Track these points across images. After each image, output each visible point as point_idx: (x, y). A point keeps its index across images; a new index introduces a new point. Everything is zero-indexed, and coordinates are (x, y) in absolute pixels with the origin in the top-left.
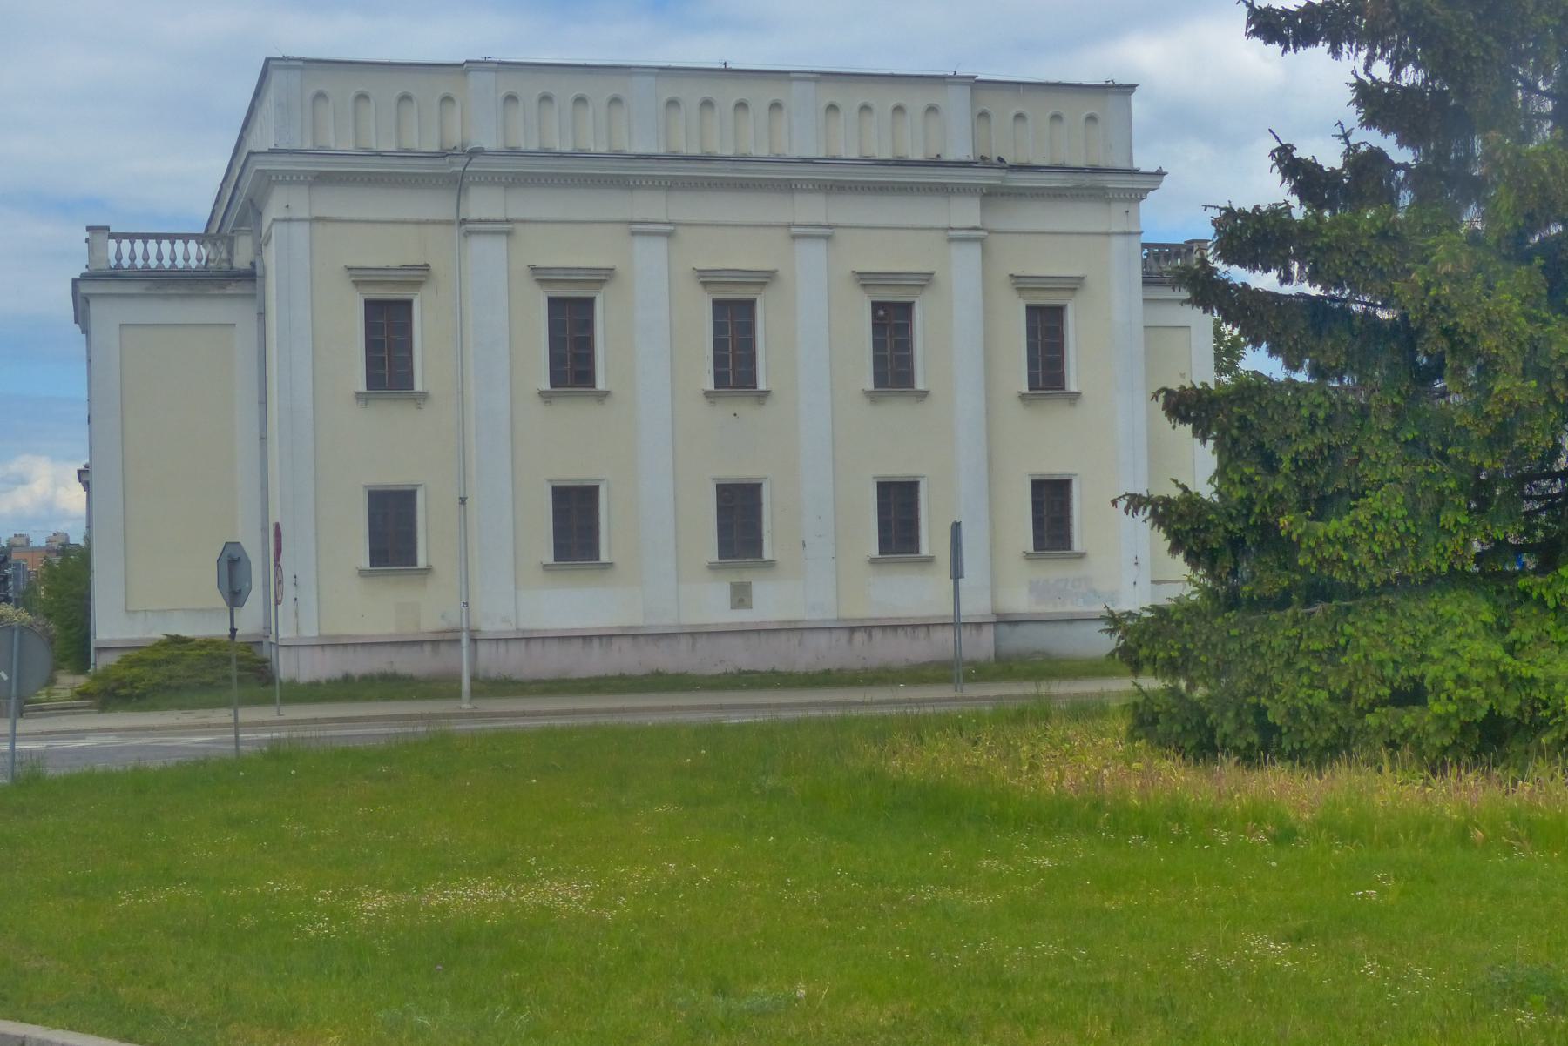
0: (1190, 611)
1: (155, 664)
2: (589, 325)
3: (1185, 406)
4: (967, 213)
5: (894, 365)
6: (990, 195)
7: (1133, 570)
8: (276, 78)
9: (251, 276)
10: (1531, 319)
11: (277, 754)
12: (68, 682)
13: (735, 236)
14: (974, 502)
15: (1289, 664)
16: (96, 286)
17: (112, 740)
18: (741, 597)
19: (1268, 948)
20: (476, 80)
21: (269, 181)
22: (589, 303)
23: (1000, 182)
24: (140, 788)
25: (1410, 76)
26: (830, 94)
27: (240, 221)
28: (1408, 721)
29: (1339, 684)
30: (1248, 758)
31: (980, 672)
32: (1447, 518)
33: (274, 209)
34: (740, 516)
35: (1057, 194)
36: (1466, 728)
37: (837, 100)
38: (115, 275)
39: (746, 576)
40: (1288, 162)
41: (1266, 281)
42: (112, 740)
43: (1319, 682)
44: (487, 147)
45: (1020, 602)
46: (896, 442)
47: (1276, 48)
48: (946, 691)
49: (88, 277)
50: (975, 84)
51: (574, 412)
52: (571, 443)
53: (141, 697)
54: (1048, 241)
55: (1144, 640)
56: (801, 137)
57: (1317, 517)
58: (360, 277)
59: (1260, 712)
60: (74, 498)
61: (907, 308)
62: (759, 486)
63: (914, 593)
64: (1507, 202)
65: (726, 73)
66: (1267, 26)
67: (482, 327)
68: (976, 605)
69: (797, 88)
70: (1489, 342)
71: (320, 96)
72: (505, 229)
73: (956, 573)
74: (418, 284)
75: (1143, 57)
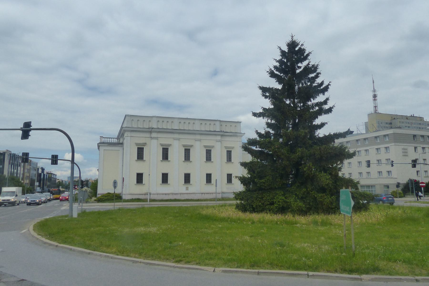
0: (244, 192)
1: (106, 196)
2: (168, 151)
3: (244, 164)
4: (219, 138)
5: (187, 157)
6: (222, 136)
7: (239, 187)
8: (127, 117)
9: (122, 144)
10: (288, 154)
11: (119, 209)
12: (94, 198)
13: (188, 140)
14: (219, 177)
15: (256, 199)
16: (99, 145)
17: (98, 207)
18: (187, 189)
19: (247, 238)
21: (125, 131)
22: (168, 149)
23: (223, 134)
24: (99, 214)
25: (273, 122)
26: (201, 122)
27: (121, 136)
28: (272, 207)
29: (263, 202)
30: (251, 212)
31: (219, 200)
32: (277, 180)
33: (126, 135)
34: (187, 178)
35: (231, 136)
36: (279, 208)
38: (103, 143)
39: (188, 186)
40: (257, 133)
41: (254, 148)
42: (98, 207)
43: (260, 202)
44: (154, 127)
45: (225, 190)
46: (209, 168)
47: (256, 117)
48: (215, 202)
49: (100, 143)
50: (220, 121)
51: (165, 163)
52: (165, 167)
53: (104, 201)
54: (230, 142)
55: (238, 196)
56: (197, 127)
57: (260, 179)
58: (137, 144)
59: (252, 205)
60: (97, 173)
61: (211, 150)
63: (211, 188)
64: (285, 138)
65: (187, 119)
66: (255, 114)
67: (153, 152)
68: (219, 190)
69: (196, 121)
70: (282, 157)
72: (157, 138)
73: (216, 186)
74: (145, 145)
75: (241, 118)
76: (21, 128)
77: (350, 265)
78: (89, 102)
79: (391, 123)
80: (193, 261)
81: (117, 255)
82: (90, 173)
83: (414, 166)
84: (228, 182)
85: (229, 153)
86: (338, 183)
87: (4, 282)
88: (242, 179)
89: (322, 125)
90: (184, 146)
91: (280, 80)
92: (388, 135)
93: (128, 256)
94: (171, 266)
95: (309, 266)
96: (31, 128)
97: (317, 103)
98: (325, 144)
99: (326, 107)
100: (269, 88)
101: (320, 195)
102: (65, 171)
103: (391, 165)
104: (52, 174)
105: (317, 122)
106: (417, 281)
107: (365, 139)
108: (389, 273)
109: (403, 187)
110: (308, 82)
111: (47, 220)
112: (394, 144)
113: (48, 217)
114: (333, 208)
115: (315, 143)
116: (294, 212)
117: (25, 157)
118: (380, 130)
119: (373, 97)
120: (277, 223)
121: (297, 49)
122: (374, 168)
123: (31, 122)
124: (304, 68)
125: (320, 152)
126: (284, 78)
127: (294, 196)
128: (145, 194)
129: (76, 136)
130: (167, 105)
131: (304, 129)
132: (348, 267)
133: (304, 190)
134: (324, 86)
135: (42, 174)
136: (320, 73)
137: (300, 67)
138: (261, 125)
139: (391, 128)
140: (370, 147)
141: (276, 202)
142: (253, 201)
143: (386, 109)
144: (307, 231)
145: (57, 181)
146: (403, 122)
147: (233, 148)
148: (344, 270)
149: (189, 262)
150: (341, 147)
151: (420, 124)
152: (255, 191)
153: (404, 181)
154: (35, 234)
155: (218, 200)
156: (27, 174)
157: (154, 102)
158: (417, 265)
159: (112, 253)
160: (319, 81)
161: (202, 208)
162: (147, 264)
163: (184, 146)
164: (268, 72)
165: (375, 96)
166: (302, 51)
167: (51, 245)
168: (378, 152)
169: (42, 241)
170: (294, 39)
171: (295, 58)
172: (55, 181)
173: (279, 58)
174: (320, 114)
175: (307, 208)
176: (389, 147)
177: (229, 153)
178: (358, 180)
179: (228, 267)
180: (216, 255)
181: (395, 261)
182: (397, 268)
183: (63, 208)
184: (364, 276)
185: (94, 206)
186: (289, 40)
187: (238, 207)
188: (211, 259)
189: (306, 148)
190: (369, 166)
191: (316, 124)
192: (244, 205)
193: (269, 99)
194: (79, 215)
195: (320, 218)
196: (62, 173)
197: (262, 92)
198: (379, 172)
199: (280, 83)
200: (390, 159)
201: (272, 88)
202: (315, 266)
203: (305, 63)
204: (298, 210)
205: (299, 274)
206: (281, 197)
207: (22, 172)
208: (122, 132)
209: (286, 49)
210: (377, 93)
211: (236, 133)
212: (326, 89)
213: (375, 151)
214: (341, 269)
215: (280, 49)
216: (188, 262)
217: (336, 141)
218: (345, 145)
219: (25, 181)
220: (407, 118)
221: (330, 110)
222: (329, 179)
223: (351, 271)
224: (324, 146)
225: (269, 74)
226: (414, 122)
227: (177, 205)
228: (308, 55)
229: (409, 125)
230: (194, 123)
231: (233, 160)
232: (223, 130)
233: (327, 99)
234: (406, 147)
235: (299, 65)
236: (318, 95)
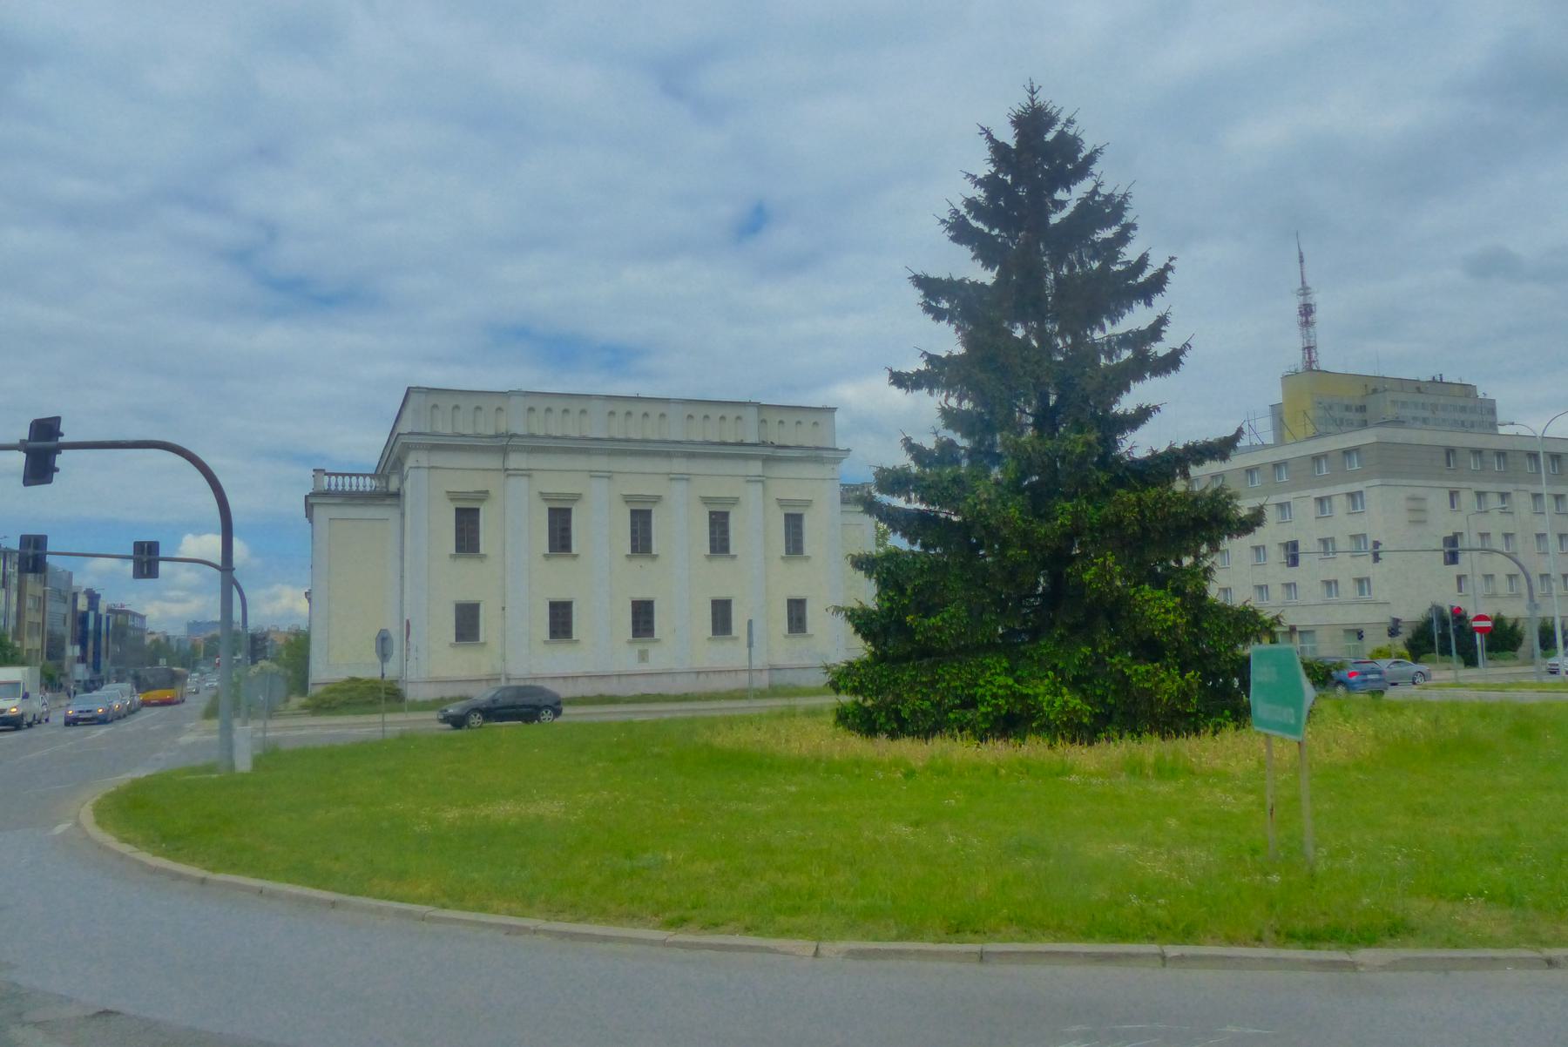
0: (865, 664)
2: (568, 521)
3: (864, 564)
4: (755, 468)
6: (767, 460)
9: (397, 495)
10: (1024, 521)
11: (402, 737)
12: (296, 701)
13: (642, 478)
14: (759, 610)
15: (912, 689)
18: (643, 656)
19: (903, 830)
21: (407, 448)
22: (568, 511)
23: (771, 454)
25: (967, 405)
27: (394, 467)
28: (969, 716)
30: (893, 735)
31: (761, 694)
32: (986, 617)
33: (410, 462)
34: (643, 617)
36: (996, 719)
38: (327, 494)
40: (910, 446)
41: (899, 502)
43: (925, 697)
45: (780, 660)
46: (721, 579)
47: (903, 391)
49: (313, 495)
50: (759, 406)
52: (560, 579)
54: (795, 483)
55: (843, 678)
56: (595, 427)
58: (453, 496)
59: (897, 712)
60: (303, 607)
63: (730, 654)
64: (1012, 465)
65: (638, 399)
66: (899, 380)
70: (1005, 532)
72: (527, 473)
73: (750, 645)
74: (482, 500)
76: (22, 441)
77: (1321, 925)
78: (276, 338)
79: (1362, 409)
80: (732, 920)
81: (444, 907)
82: (278, 605)
83: (1452, 558)
84: (791, 630)
85: (794, 524)
86: (1206, 625)
87: (36, 1024)
88: (859, 617)
89: (1143, 414)
90: (628, 499)
91: (987, 251)
92: (1357, 449)
93: (483, 909)
94: (653, 943)
95: (1159, 926)
96: (61, 440)
97: (1125, 335)
98: (1154, 485)
99: (1160, 349)
100: (950, 282)
101: (1142, 669)
102: (178, 601)
103: (1371, 557)
104: (127, 613)
105: (1126, 404)
106: (1550, 963)
107: (1277, 466)
108: (1449, 940)
109: (1410, 636)
110: (1092, 258)
111: (138, 786)
112: (1377, 482)
113: (140, 773)
114: (1190, 715)
115: (1120, 482)
116: (1050, 730)
117: (30, 552)
118: (1328, 434)
119: (1301, 314)
120: (996, 772)
121: (1049, 137)
122: (1310, 571)
123: (57, 420)
124: (1078, 208)
125: (1141, 512)
126: (1004, 244)
127: (1051, 674)
128: (565, 678)
129: (218, 468)
130: (563, 348)
131: (1080, 431)
132: (1300, 926)
133: (1086, 650)
134: (1148, 273)
135: (92, 614)
136: (1133, 226)
137: (1061, 205)
138: (924, 417)
139: (1364, 424)
140: (1294, 495)
141: (983, 696)
142: (899, 696)
143: (1342, 356)
144: (1109, 797)
145: (148, 640)
146: (1404, 404)
147: (808, 503)
148: (1291, 937)
149: (716, 925)
150: (1216, 493)
151: (1463, 409)
152: (907, 658)
153: (1413, 611)
154: (110, 840)
155: (756, 697)
156: (32, 617)
157: (519, 335)
158: (1538, 907)
159: (419, 900)
160: (1131, 253)
161: (711, 724)
162: (563, 935)
163: (628, 499)
164: (943, 221)
165: (1307, 311)
166: (1068, 144)
167: (179, 877)
168: (1355, 507)
169: (141, 864)
170: (1041, 98)
171: (1044, 172)
172: (142, 638)
173: (985, 169)
174: (1139, 377)
175: (1095, 716)
176: (1361, 493)
177: (794, 524)
178: (1275, 613)
179: (865, 937)
180: (812, 895)
181: (1461, 896)
182: (1472, 922)
183: (186, 739)
184: (1363, 955)
185: (339, 725)
186: (1018, 101)
187: (842, 717)
188: (796, 910)
189: (1090, 500)
190: (1293, 561)
191: (1120, 412)
192: (866, 710)
193: (950, 322)
194: (257, 762)
195: (1151, 748)
196: (172, 607)
197: (927, 295)
198: (1328, 583)
199: (988, 263)
200: (1364, 536)
201: (962, 280)
202: (1181, 926)
203: (1081, 189)
204: (1065, 724)
205: (1195, 958)
206: (1001, 680)
207: (14, 609)
208: (396, 450)
209: (1008, 136)
210: (1317, 298)
211: (817, 448)
212: (1158, 283)
213: (1312, 508)
214: (1277, 933)
215: (990, 138)
216: (714, 926)
217: (1194, 471)
218: (1233, 486)
219: (26, 639)
220: (1417, 387)
221: (1171, 362)
222: (1175, 609)
223: (1312, 938)
224: (1153, 492)
225: (950, 229)
226: (1442, 401)
227: (612, 718)
228: (1091, 159)
229: (1427, 414)
230: (583, 412)
231: (809, 547)
232: (772, 436)
233: (1162, 320)
234: (1419, 492)
235: (1060, 195)
236: (1130, 307)
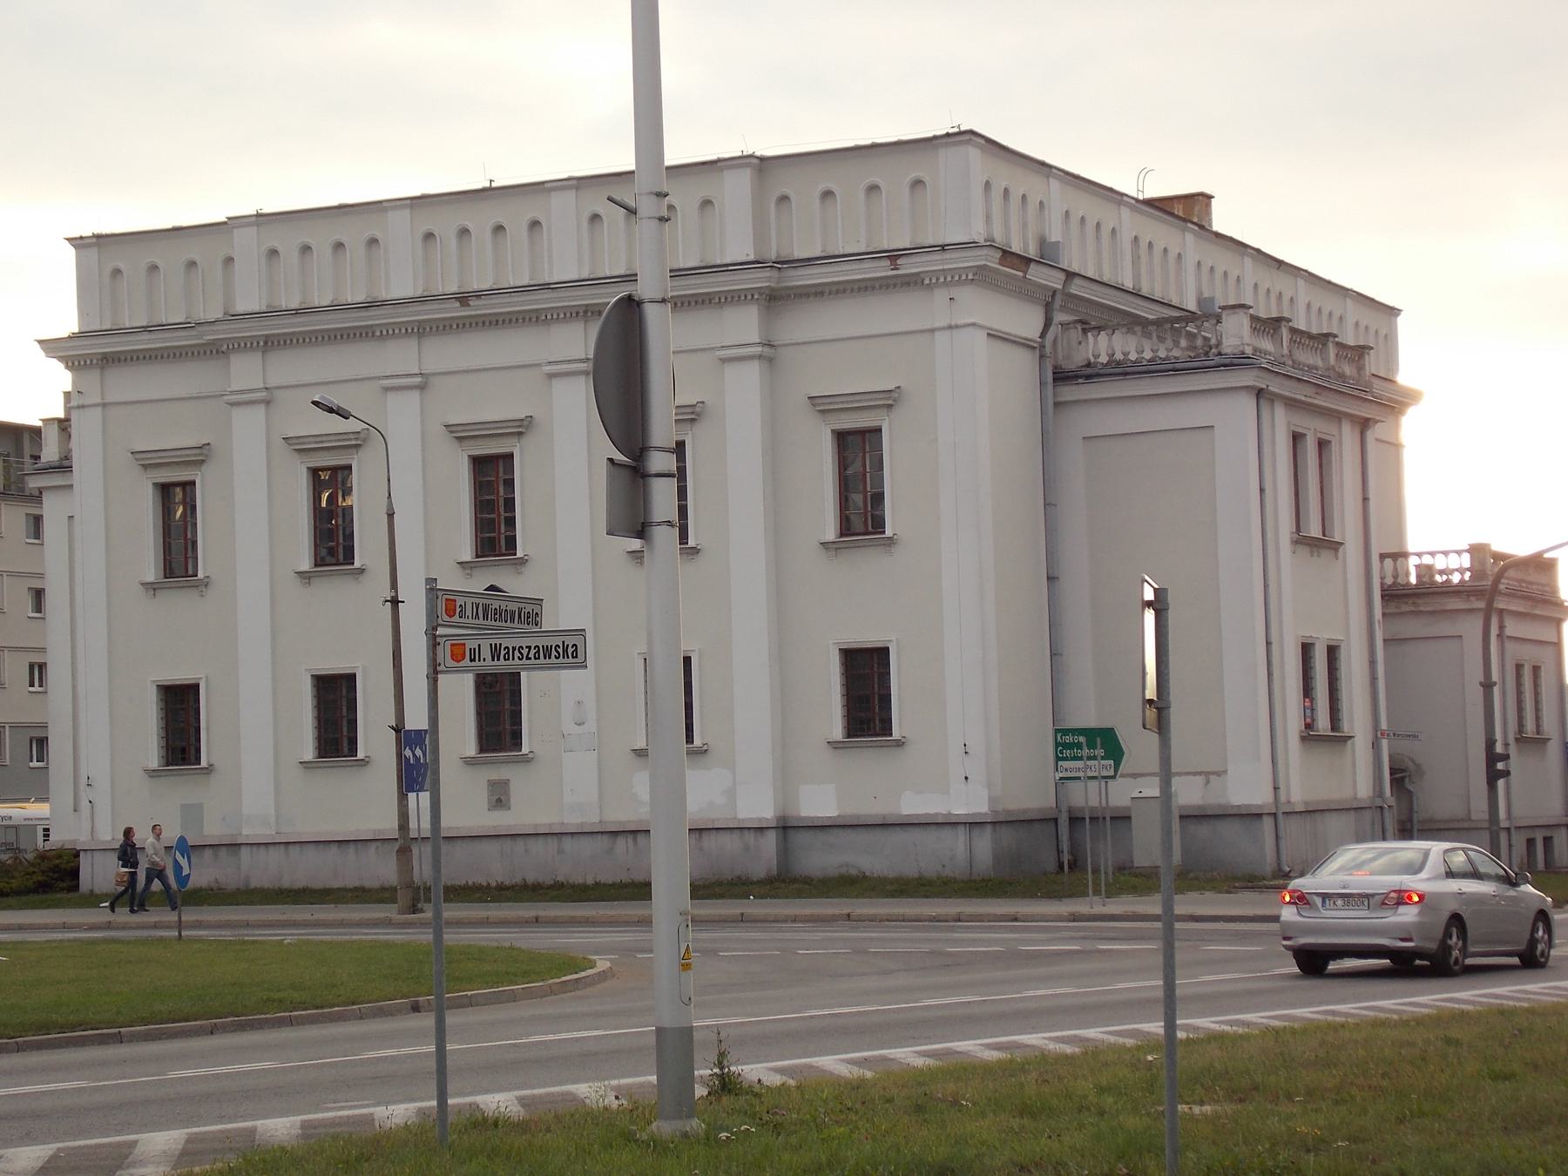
4: (744, 325)
18: (499, 797)
20: (558, 200)
37: (832, 186)
39: (503, 773)
50: (762, 165)
62: (196, 687)
71: (117, 272)
